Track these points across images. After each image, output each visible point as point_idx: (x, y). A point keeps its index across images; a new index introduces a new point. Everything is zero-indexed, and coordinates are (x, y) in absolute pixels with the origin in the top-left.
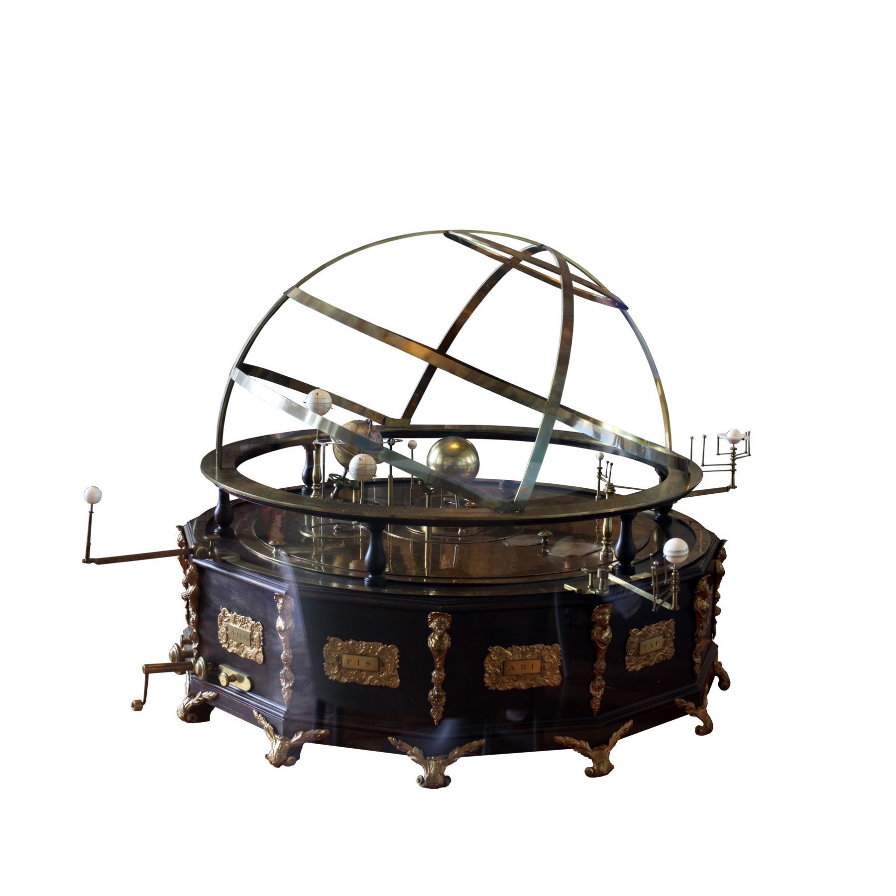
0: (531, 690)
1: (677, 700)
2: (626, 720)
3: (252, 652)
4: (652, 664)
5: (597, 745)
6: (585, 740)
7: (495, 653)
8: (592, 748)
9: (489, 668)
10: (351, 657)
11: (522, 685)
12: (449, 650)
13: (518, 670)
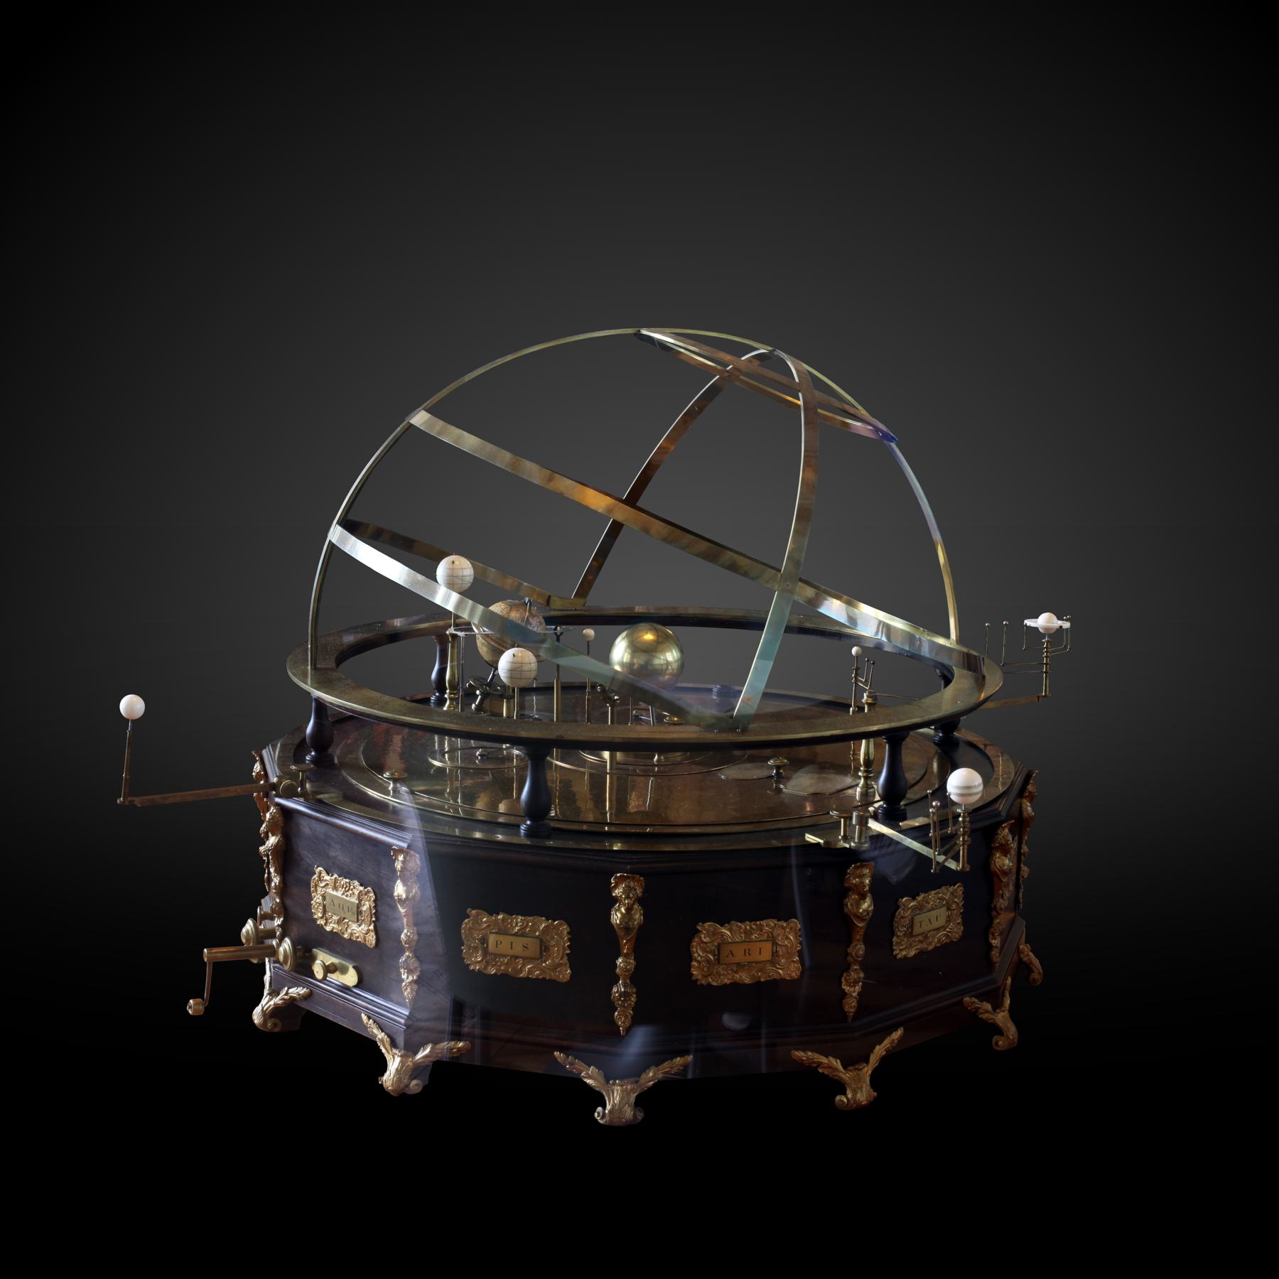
0: (757, 985)
1: (967, 999)
2: (894, 1028)
3: (360, 931)
4: (931, 948)
5: (853, 1064)
6: (835, 1057)
7: (706, 931)
8: (845, 1068)
9: (698, 953)
10: (501, 938)
11: (745, 978)
12: (641, 927)
13: (739, 957)
